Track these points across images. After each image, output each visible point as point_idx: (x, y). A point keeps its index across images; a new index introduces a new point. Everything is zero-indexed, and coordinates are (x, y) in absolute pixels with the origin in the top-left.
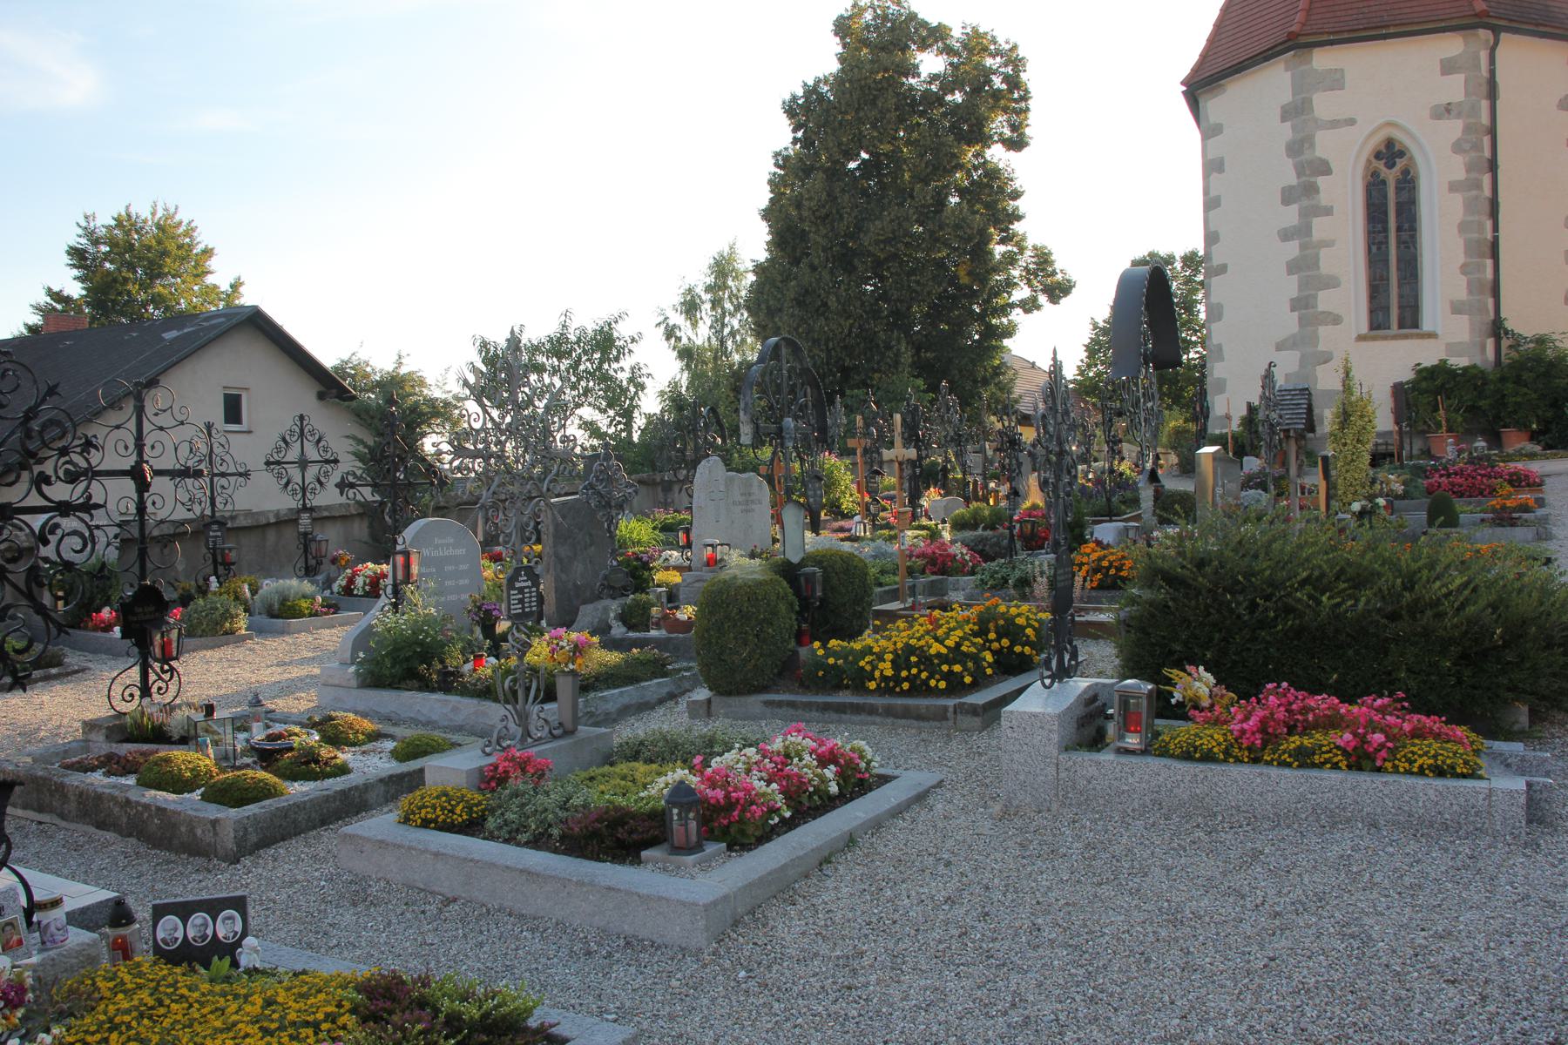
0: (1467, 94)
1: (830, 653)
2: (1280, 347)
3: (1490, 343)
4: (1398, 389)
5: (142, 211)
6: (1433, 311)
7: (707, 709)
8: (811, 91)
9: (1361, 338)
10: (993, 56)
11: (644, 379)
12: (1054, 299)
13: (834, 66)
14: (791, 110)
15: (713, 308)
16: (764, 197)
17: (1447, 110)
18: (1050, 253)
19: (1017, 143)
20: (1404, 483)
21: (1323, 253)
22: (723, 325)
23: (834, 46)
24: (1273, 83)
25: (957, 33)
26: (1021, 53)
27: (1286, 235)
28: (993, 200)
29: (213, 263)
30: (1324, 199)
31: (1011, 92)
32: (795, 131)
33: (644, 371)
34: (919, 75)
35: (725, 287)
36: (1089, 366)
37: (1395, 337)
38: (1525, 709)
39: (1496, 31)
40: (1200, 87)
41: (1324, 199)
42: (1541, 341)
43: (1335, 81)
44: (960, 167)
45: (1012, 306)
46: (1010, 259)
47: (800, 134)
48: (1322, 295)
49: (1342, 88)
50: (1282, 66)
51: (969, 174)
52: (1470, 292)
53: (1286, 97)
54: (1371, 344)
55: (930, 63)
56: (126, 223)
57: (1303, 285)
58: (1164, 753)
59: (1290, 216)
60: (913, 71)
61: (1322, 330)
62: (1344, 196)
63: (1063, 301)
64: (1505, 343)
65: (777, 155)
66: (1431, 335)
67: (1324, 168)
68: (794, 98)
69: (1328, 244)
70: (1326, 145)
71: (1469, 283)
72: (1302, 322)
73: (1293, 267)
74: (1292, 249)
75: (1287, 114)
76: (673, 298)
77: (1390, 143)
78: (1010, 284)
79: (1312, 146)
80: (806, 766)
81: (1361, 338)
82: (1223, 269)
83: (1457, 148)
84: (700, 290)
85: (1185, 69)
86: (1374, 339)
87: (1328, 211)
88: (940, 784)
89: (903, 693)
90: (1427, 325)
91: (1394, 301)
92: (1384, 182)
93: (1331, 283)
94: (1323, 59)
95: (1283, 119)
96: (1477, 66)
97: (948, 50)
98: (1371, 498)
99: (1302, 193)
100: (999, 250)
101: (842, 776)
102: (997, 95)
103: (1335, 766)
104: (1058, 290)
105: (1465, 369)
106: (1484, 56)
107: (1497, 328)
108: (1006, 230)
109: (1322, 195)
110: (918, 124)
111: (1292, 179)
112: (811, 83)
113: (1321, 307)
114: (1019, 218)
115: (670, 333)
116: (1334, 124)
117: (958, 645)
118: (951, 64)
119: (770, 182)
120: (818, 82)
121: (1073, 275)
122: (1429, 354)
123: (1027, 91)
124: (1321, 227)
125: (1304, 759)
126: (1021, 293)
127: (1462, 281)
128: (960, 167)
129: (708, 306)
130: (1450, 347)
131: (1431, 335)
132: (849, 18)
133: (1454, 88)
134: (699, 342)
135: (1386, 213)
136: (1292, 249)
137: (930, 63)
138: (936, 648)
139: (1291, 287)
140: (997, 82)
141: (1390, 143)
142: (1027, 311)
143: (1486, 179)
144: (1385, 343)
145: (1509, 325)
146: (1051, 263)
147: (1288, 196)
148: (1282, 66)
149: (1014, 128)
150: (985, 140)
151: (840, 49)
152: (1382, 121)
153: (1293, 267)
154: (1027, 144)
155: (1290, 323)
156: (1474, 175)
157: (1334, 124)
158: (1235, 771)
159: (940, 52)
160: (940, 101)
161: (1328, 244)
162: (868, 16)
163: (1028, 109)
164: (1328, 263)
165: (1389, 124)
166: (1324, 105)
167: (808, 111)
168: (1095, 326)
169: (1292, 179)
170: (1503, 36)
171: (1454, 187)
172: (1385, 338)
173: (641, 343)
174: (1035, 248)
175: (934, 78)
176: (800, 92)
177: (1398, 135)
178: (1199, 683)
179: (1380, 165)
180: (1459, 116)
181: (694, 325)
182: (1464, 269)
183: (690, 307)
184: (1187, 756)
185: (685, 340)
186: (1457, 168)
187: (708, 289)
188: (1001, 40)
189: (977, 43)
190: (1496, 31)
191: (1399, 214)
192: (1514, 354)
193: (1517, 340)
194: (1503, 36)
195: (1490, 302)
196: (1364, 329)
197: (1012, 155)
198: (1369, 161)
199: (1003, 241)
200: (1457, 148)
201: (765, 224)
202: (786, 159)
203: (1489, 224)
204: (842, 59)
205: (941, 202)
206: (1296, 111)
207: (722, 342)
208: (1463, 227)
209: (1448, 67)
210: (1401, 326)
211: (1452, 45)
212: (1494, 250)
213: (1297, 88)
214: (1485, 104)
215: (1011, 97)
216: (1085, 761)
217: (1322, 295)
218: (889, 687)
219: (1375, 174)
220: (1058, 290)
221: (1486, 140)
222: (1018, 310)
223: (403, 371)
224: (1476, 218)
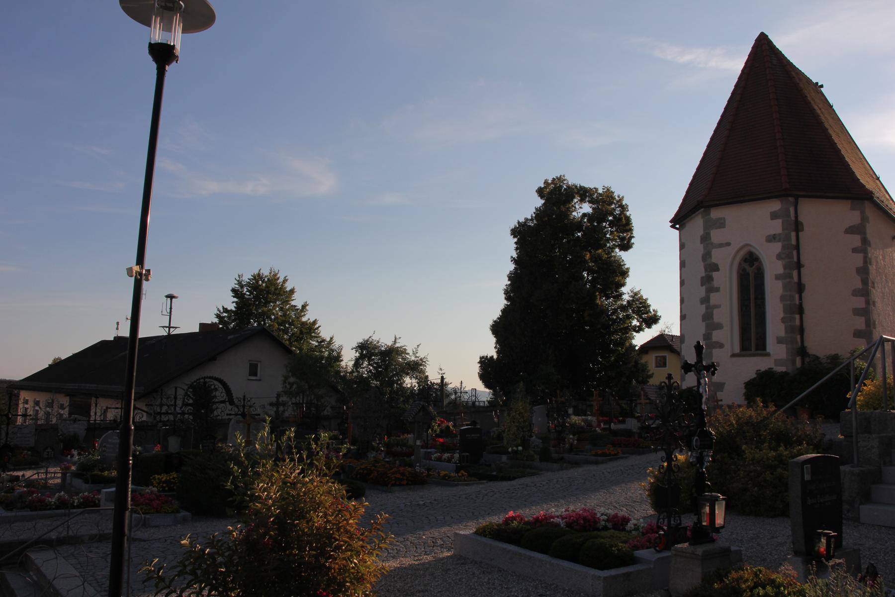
0: (783, 229)
5: (266, 272)
6: (771, 345)
7: (611, 546)
14: (514, 232)
17: (772, 238)
21: (715, 311)
24: (697, 224)
25: (600, 191)
29: (295, 296)
37: (754, 355)
39: (797, 198)
40: (678, 221)
41: (716, 283)
43: (721, 224)
48: (715, 333)
49: (724, 227)
50: (700, 216)
52: (786, 332)
54: (741, 359)
56: (258, 277)
66: (768, 355)
67: (716, 268)
69: (718, 307)
70: (717, 256)
71: (786, 328)
81: (733, 355)
83: (779, 257)
85: (672, 216)
86: (744, 356)
90: (768, 350)
91: (752, 339)
92: (748, 274)
93: (719, 327)
94: (715, 214)
96: (788, 215)
106: (792, 210)
107: (802, 351)
113: (714, 339)
116: (721, 245)
122: (761, 364)
124: (714, 298)
130: (778, 362)
133: (777, 227)
143: (795, 273)
144: (748, 358)
148: (700, 216)
152: (742, 244)
157: (721, 245)
161: (718, 307)
164: (719, 316)
166: (717, 236)
167: (521, 232)
171: (777, 277)
179: (746, 266)
180: (779, 241)
195: (799, 337)
196: (737, 350)
198: (740, 264)
200: (779, 257)
203: (797, 296)
208: (782, 298)
209: (774, 216)
210: (757, 349)
211: (775, 205)
212: (800, 310)
214: (793, 234)
217: (715, 333)
221: (795, 253)
223: (397, 345)
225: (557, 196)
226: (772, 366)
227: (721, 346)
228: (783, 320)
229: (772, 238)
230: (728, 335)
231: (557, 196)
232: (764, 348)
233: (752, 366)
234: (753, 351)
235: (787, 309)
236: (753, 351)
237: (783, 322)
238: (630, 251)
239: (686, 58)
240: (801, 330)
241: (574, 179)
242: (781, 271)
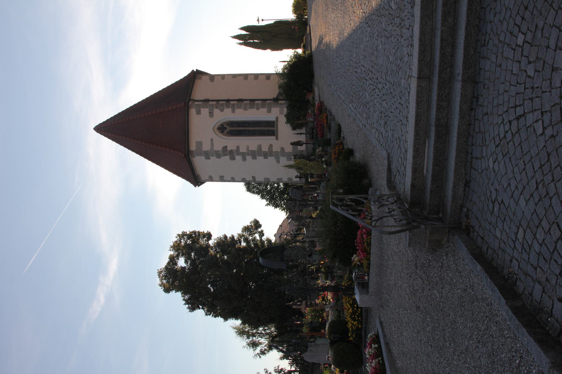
1: (352, 336)
2: (278, 162)
3: (280, 102)
4: (294, 129)
6: (271, 117)
8: (187, 302)
9: (277, 139)
10: (181, 242)
11: (280, 368)
12: (260, 226)
13: (179, 294)
15: (255, 337)
16: (220, 319)
17: (211, 114)
18: (245, 227)
19: (209, 236)
20: (319, 147)
21: (251, 149)
22: (261, 333)
23: (173, 293)
24: (199, 162)
25: (172, 253)
26: (181, 233)
27: (244, 159)
28: (227, 244)
30: (234, 148)
31: (192, 237)
32: (199, 308)
33: (277, 368)
34: (185, 267)
35: (248, 332)
36: (282, 207)
38: (364, 181)
39: (190, 100)
40: (197, 181)
41: (234, 148)
42: (280, 87)
43: (199, 144)
44: (216, 255)
45: (261, 240)
46: (246, 240)
47: (201, 307)
49: (202, 142)
50: (194, 159)
51: (217, 252)
52: (265, 107)
53: (203, 158)
55: (181, 262)
57: (260, 155)
58: (369, 272)
59: (238, 158)
60: (183, 268)
61: (274, 150)
62: (233, 142)
63: (261, 223)
64: (280, 98)
65: (206, 314)
66: (277, 118)
67: (225, 148)
68: (189, 308)
69: (248, 147)
70: (218, 147)
72: (271, 155)
73: (254, 158)
74: (249, 158)
75: (208, 158)
76: (251, 352)
77: (219, 129)
78: (254, 239)
79: (218, 151)
80: (372, 351)
81: (277, 139)
82: (254, 177)
83: (222, 110)
84: (248, 341)
87: (238, 147)
88: (379, 317)
89: (362, 319)
90: (274, 119)
91: (267, 129)
92: (230, 131)
93: (260, 147)
94: (193, 147)
95: (209, 159)
97: (178, 256)
98: (322, 162)
99: (232, 154)
100: (244, 244)
101: (375, 343)
102: (193, 242)
103: (371, 238)
104: (257, 224)
105: (287, 110)
106: (196, 103)
107: (276, 100)
108: (237, 241)
109: (233, 149)
110: (201, 268)
111: (228, 157)
112: (184, 302)
113: (267, 150)
114: (233, 237)
115: (263, 353)
116: (212, 145)
117: (350, 305)
118: (182, 255)
119: (215, 317)
120: (184, 300)
121: (252, 219)
122: (282, 120)
123: (193, 232)
124: (243, 150)
125: (369, 244)
126: (257, 236)
127: (261, 109)
128: (216, 255)
129: (254, 338)
130: (281, 113)
131: (277, 118)
132: (164, 287)
133: (205, 111)
134: (267, 342)
135: (240, 130)
136: (249, 158)
137: (181, 262)
138: (350, 310)
139: (260, 159)
140: (189, 242)
141: (219, 129)
142: (263, 235)
143: (232, 102)
145: (275, 96)
146: (248, 226)
147: (232, 158)
148: (194, 159)
149: (204, 237)
150: (208, 246)
151: (174, 291)
153: (254, 158)
154: (210, 233)
155: (272, 159)
156: (230, 106)
157: (212, 145)
158: (372, 259)
159: (178, 259)
160: (195, 260)
161: (248, 147)
162: (165, 281)
163: (199, 232)
164: (254, 148)
165: (213, 129)
166: (206, 147)
167: (193, 305)
168: (268, 205)
169: (228, 157)
170: (191, 98)
171: (233, 111)
172: (277, 132)
173: (268, 369)
174: (243, 231)
175: (186, 262)
176: (187, 306)
177: (217, 126)
178: (355, 258)
179: (225, 131)
180: (213, 110)
181: (261, 343)
182: (258, 109)
183: (254, 345)
184: (369, 268)
185: (266, 348)
186: (228, 111)
187: (248, 338)
188: (176, 239)
189: (176, 247)
190: (190, 100)
191: (240, 127)
192: (284, 96)
193: (280, 94)
194: (191, 98)
195: (268, 102)
196: (274, 137)
197: (213, 238)
198: (224, 135)
199: (240, 242)
200: (222, 110)
201: (229, 320)
202: (208, 311)
203: (245, 102)
204: (177, 291)
205: (226, 262)
206: (207, 155)
207: (267, 334)
208: (245, 109)
209: (199, 113)
211: (193, 111)
212: (253, 101)
213: (200, 155)
214: (210, 103)
215: (194, 236)
216: (371, 288)
218: (360, 322)
219: (228, 133)
220: (257, 224)
221: (220, 102)
222: (263, 238)
224: (243, 106)
225: (172, 279)
226: (283, 115)
227: (271, 146)
228: (258, 109)
229: (211, 114)
230: (265, 142)
231: (172, 279)
232: (273, 122)
233: (284, 128)
234: (275, 129)
235: (252, 107)
236: (275, 129)
237: (263, 198)
238: (212, 233)
239: (102, 298)
240: (264, 100)
241: (164, 262)
242: (230, 110)
